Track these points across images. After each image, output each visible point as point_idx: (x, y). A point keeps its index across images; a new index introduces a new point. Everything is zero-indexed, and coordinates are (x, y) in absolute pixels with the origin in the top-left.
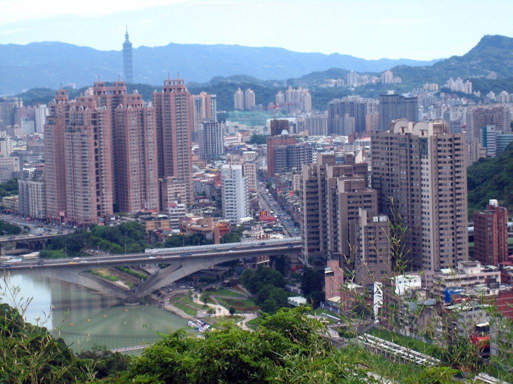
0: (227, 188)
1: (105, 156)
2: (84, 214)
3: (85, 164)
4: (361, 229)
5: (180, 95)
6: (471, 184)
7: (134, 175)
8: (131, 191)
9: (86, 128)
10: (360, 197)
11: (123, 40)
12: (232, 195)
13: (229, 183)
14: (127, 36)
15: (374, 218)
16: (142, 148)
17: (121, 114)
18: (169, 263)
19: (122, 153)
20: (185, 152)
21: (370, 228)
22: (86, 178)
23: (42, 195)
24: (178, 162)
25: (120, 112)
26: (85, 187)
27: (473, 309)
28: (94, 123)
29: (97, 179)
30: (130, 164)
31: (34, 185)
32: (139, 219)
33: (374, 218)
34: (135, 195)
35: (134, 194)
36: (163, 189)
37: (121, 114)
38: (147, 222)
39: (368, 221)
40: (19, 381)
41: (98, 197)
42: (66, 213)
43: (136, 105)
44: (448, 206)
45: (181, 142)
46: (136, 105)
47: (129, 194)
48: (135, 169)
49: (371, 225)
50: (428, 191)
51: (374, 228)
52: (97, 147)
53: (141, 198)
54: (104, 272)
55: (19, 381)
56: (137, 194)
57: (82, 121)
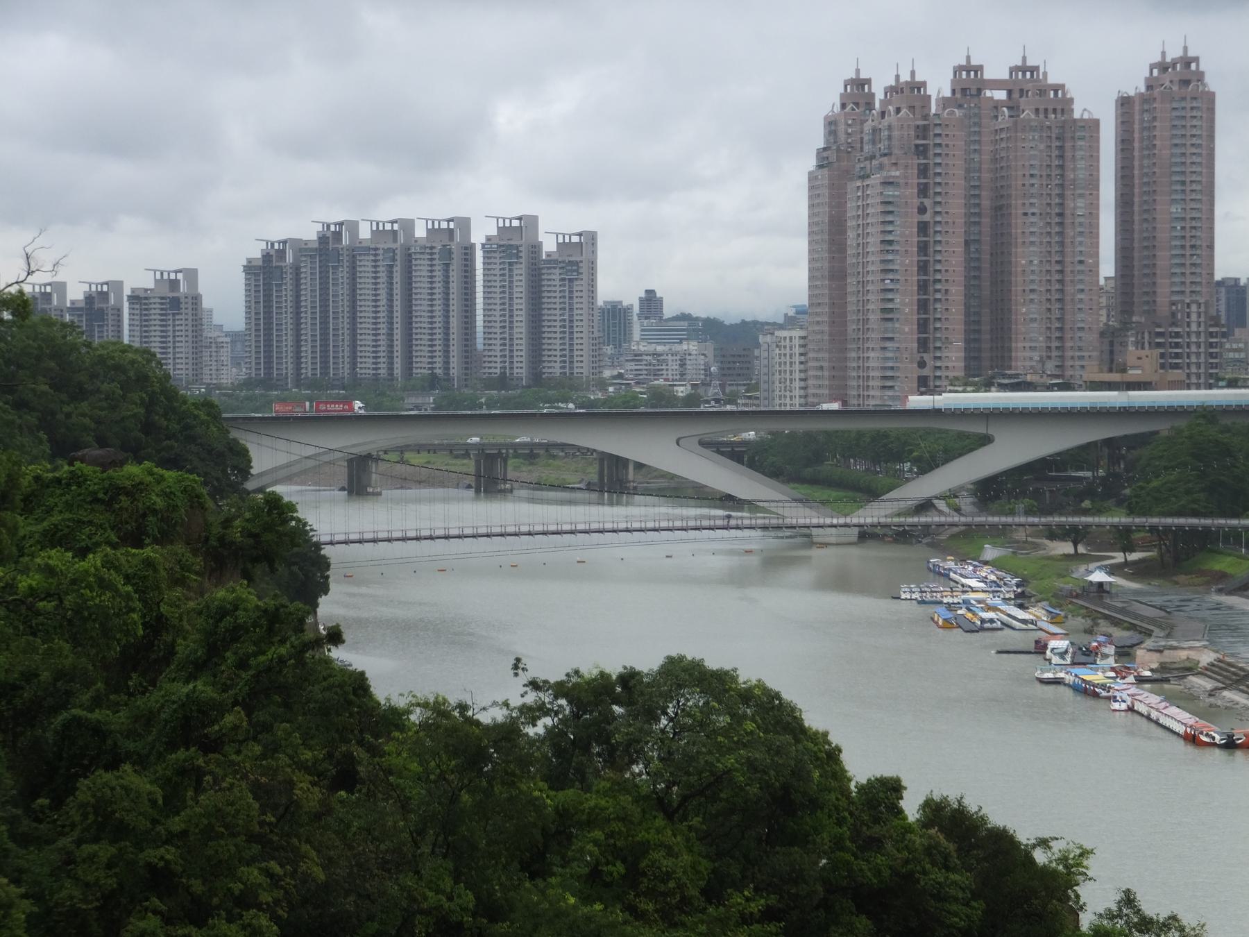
1: (947, 243)
2: (882, 397)
6: (361, 692)
7: (1032, 301)
9: (896, 164)
16: (1054, 344)
17: (1003, 135)
18: (979, 428)
19: (1002, 243)
20: (1192, 255)
23: (800, 371)
24: (1173, 284)
25: (1002, 130)
26: (889, 325)
28: (921, 151)
29: (923, 306)
30: (1019, 269)
31: (785, 338)
34: (1031, 358)
35: (1028, 354)
36: (1117, 348)
37: (1003, 135)
40: (421, 925)
41: (925, 355)
43: (1046, 110)
45: (1183, 228)
46: (1046, 110)
47: (1013, 354)
48: (1035, 287)
52: (927, 217)
53: (1049, 348)
54: (1202, 684)
55: (421, 925)
57: (889, 147)
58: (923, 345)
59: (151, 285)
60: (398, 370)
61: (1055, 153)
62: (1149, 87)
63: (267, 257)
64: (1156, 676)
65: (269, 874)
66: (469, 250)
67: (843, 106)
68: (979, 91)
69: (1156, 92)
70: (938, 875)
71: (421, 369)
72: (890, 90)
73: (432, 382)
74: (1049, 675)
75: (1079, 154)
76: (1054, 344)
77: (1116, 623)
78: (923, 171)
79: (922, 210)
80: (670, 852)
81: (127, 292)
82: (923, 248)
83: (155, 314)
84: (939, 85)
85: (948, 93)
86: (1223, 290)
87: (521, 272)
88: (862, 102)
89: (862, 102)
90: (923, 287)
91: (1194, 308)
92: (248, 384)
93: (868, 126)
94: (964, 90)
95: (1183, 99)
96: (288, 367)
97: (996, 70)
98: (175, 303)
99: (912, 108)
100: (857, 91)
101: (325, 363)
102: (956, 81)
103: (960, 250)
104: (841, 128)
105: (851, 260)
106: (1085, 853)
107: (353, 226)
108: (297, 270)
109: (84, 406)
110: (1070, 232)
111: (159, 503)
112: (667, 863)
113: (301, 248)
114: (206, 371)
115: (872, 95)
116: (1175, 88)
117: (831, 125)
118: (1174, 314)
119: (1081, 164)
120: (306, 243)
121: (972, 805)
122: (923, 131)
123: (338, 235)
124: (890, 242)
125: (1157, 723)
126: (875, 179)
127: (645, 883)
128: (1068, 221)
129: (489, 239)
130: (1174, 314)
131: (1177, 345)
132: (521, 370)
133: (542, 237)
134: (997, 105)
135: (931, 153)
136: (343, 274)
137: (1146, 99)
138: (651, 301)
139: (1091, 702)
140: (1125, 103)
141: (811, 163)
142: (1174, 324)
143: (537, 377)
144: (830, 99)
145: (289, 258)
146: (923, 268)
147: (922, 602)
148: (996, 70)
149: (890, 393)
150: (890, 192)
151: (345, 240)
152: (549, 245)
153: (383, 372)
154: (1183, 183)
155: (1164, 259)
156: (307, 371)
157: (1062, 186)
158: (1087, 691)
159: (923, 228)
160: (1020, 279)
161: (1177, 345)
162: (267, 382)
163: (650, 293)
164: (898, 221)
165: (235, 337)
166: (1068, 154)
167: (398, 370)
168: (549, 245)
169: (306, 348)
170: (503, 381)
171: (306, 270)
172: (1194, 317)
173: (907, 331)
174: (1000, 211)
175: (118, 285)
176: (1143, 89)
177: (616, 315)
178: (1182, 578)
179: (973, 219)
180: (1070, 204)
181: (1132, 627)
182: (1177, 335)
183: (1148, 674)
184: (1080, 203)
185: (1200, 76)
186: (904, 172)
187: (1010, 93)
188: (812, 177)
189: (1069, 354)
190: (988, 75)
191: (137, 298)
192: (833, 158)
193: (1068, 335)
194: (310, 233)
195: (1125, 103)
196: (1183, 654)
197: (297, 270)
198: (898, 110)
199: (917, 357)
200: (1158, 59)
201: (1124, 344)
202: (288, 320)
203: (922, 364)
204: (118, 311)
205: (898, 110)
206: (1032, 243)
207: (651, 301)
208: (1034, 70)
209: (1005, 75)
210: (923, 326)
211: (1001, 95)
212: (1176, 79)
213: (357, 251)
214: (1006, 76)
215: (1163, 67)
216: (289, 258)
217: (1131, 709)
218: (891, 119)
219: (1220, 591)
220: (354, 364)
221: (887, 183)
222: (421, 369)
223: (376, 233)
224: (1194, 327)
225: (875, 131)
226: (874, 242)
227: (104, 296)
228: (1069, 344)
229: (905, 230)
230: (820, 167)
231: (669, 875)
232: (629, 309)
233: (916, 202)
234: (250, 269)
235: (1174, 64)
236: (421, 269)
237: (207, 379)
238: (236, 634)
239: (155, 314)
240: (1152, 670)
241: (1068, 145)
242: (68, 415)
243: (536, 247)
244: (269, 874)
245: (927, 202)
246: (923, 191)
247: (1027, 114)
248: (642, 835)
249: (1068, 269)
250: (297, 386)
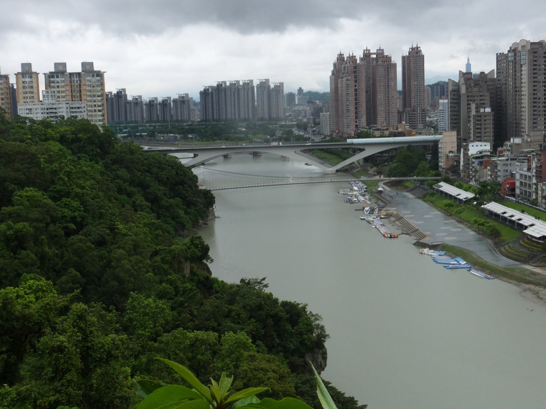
0: (440, 115)
3: (348, 98)
4: (471, 117)
5: (417, 57)
8: (379, 116)
10: (477, 96)
11: (466, 62)
12: (443, 119)
13: (441, 111)
14: (468, 60)
15: (481, 109)
16: (387, 116)
18: (362, 147)
21: (478, 116)
22: (349, 107)
27: (509, 160)
28: (355, 72)
29: (356, 108)
32: (371, 130)
33: (481, 109)
35: (381, 119)
36: (402, 116)
38: (375, 132)
39: (477, 112)
42: (339, 131)
44: (541, 103)
49: (478, 114)
50: (525, 90)
51: (481, 116)
52: (357, 87)
56: (383, 119)
58: (356, 117)
59: (178, 98)
60: (237, 117)
61: (386, 71)
62: (409, 54)
63: (205, 90)
64: (385, 217)
65: (191, 324)
66: (253, 87)
67: (337, 60)
68: (370, 55)
69: (411, 55)
70: (281, 313)
71: (242, 116)
72: (348, 57)
73: (245, 120)
74: (363, 218)
75: (392, 71)
76: (387, 116)
77: (382, 201)
78: (356, 77)
79: (355, 86)
80: (243, 315)
81: (172, 99)
82: (356, 95)
83: (179, 104)
84: (359, 55)
85: (362, 56)
86: (439, 86)
87: (265, 92)
88: (342, 59)
89: (342, 59)
90: (356, 104)
91: (418, 107)
92: (201, 121)
93: (343, 66)
94: (366, 55)
95: (417, 57)
96: (211, 117)
97: (373, 50)
98: (183, 102)
99: (353, 62)
100: (341, 58)
101: (219, 116)
102: (364, 53)
103: (365, 95)
104: (337, 66)
105: (339, 98)
106: (307, 305)
107: (225, 82)
108: (212, 93)
109: (164, 173)
110: (390, 90)
111: (177, 252)
112: (243, 316)
113: (212, 87)
114: (191, 116)
115: (344, 58)
116: (415, 54)
117: (335, 65)
118: (414, 109)
119: (392, 74)
120: (214, 87)
121: (288, 301)
122: (355, 67)
123: (221, 85)
124: (348, 94)
125: (379, 231)
126: (345, 79)
127: (240, 318)
128: (390, 87)
129: (257, 85)
130: (414, 109)
131: (415, 116)
132: (266, 116)
133: (270, 84)
134: (373, 59)
135: (357, 72)
136: (223, 94)
137: (408, 57)
138: (300, 90)
139: (369, 224)
140: (403, 58)
141: (330, 74)
142: (414, 111)
143: (270, 119)
144: (334, 59)
145: (210, 90)
146: (356, 99)
147: (344, 194)
148: (373, 50)
149: (349, 129)
150: (348, 82)
151: (223, 86)
152: (272, 86)
153: (233, 117)
154: (417, 77)
155: (413, 94)
156: (215, 118)
157: (388, 79)
158: (369, 222)
159: (356, 90)
160: (379, 101)
161: (415, 116)
162: (206, 121)
163: (300, 88)
164: (350, 89)
165: (199, 102)
166: (389, 72)
167: (237, 117)
168: (272, 86)
169: (215, 112)
170: (262, 119)
171: (214, 93)
172: (419, 110)
173: (352, 114)
174: (374, 85)
175: (169, 98)
176: (408, 54)
177: (291, 96)
178: (399, 187)
179: (367, 86)
180: (390, 83)
181: (384, 202)
182: (415, 114)
183: (383, 217)
184: (393, 83)
185: (421, 51)
186: (351, 78)
187: (377, 56)
188: (330, 77)
189: (390, 118)
190: (371, 52)
191: (175, 101)
192: (335, 73)
193: (390, 114)
194: (215, 84)
195: (403, 58)
196: (391, 211)
197: (212, 93)
198: (350, 63)
199: (355, 120)
200: (411, 47)
201: (403, 115)
202: (210, 105)
203: (356, 122)
204: (170, 104)
205: (350, 63)
206: (382, 93)
207: (300, 90)
208: (383, 50)
209: (376, 52)
210: (356, 113)
211: (374, 56)
212: (415, 52)
213: (226, 89)
214: (376, 52)
215: (412, 49)
216: (210, 90)
217: (376, 227)
218: (348, 64)
219: (406, 191)
220: (226, 116)
221: (347, 80)
222: (242, 116)
223: (231, 84)
224: (419, 112)
225: (345, 67)
226: (345, 93)
227: (166, 100)
228: (390, 116)
229: (352, 91)
230: (332, 75)
231: (243, 317)
232: (295, 94)
233: (354, 84)
234: (201, 93)
235: (415, 48)
236: (242, 93)
237: (192, 119)
238: (187, 291)
239: (179, 104)
240: (384, 215)
241: (389, 69)
242: (161, 175)
243: (269, 86)
244: (191, 324)
245: (357, 84)
246: (356, 81)
247: (380, 62)
248: (240, 312)
249: (390, 98)
250: (213, 121)
